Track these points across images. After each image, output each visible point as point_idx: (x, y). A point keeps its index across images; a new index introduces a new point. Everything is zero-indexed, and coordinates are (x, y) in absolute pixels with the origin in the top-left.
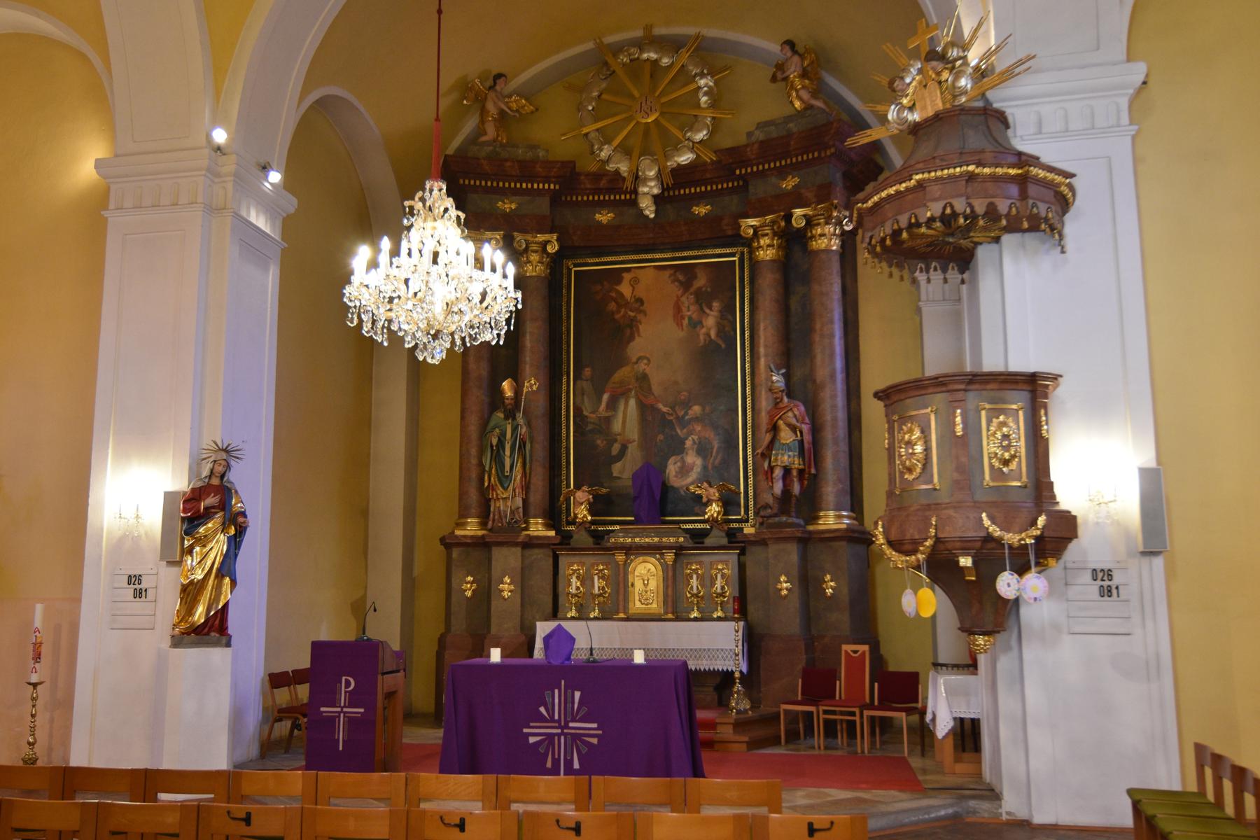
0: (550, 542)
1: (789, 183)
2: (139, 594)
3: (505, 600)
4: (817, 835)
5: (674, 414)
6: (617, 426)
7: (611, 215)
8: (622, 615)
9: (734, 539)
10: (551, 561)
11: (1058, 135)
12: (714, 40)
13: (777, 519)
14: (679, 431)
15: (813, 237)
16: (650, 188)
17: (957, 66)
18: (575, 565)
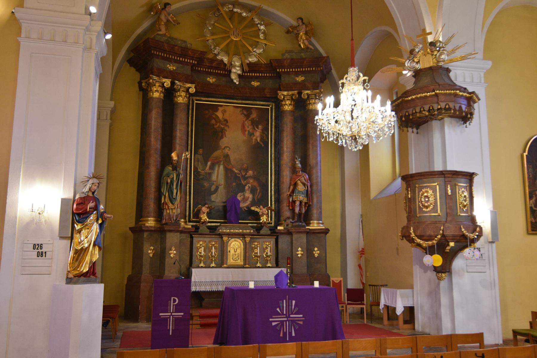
1: (300, 79)
2: (41, 254)
3: (172, 258)
5: (241, 174)
6: (214, 178)
7: (214, 80)
8: (225, 266)
9: (273, 232)
10: (189, 239)
12: (266, 10)
13: (297, 224)
15: (310, 104)
16: (236, 71)
18: (201, 242)
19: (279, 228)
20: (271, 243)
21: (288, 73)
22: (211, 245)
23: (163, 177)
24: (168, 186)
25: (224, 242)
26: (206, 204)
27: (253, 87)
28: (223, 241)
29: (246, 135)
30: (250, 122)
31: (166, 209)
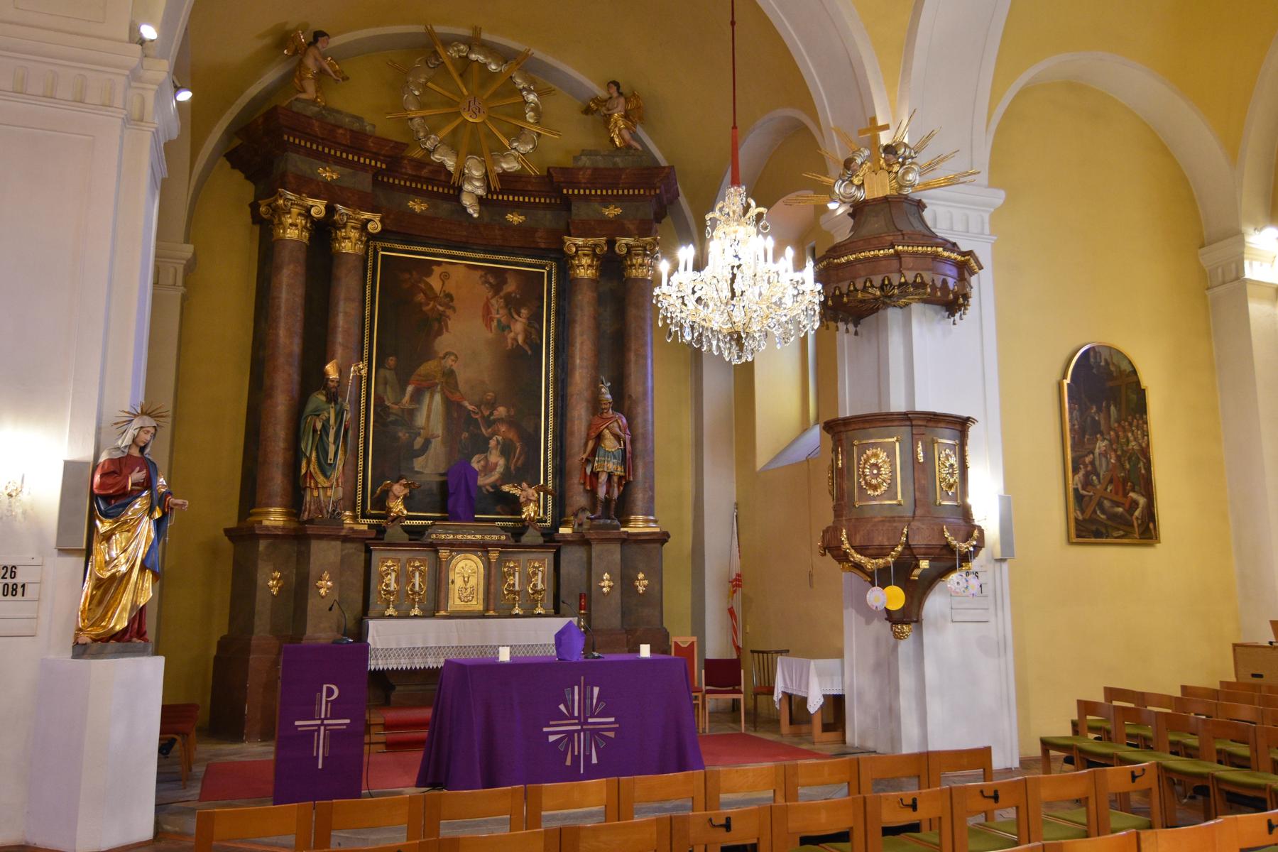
0: (365, 537)
1: (612, 212)
3: (322, 597)
4: (1137, 780)
6: (420, 420)
8: (442, 613)
9: (550, 539)
11: (960, 233)
14: (483, 430)
16: (473, 189)
17: (907, 163)
18: (390, 561)
19: (562, 530)
20: (545, 563)
21: (586, 198)
22: (411, 569)
23: (305, 418)
24: (317, 438)
25: (441, 561)
26: (401, 478)
27: (510, 226)
28: (438, 558)
29: (493, 329)
30: (502, 300)
31: (310, 487)
